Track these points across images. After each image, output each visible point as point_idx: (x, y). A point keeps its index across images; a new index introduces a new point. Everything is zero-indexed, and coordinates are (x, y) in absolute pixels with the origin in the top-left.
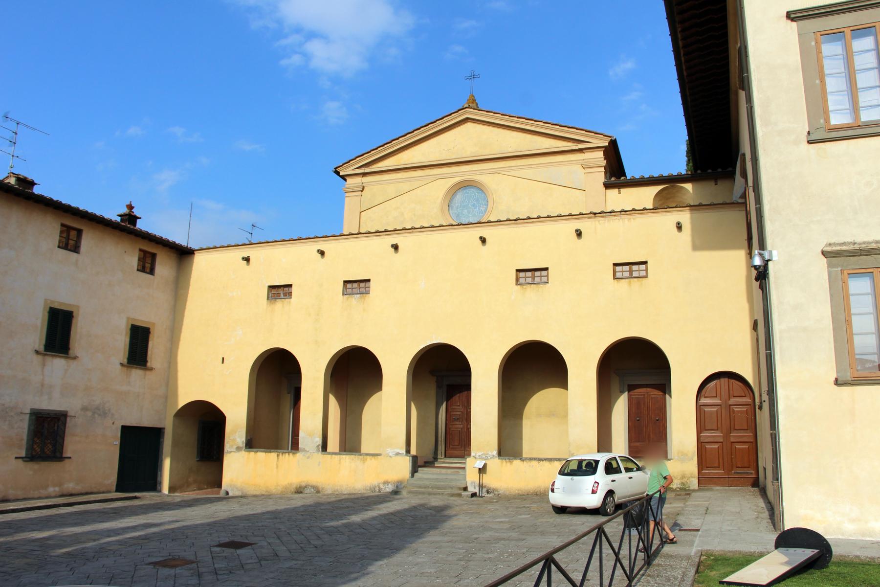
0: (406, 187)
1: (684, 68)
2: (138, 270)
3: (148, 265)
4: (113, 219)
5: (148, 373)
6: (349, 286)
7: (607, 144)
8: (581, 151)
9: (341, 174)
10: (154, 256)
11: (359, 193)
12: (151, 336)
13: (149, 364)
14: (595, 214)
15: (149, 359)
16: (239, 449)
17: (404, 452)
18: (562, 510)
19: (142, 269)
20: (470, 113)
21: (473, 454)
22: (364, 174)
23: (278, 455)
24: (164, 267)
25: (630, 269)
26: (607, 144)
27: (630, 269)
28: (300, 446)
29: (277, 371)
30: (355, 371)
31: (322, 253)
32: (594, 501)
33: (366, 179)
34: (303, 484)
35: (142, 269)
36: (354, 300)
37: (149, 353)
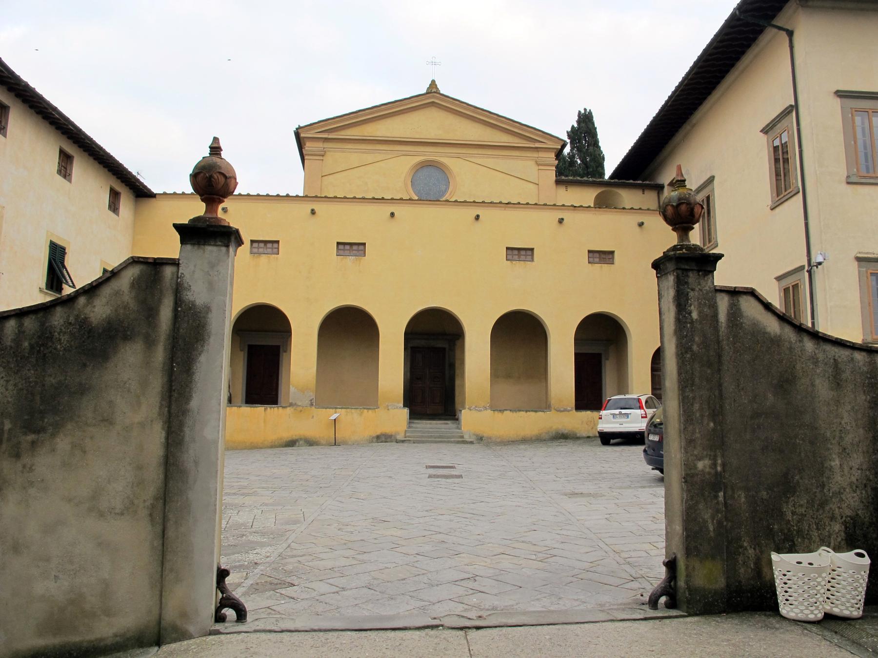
0: (369, 158)
6: (341, 247)
22: (326, 140)
34: (294, 438)
36: (349, 261)
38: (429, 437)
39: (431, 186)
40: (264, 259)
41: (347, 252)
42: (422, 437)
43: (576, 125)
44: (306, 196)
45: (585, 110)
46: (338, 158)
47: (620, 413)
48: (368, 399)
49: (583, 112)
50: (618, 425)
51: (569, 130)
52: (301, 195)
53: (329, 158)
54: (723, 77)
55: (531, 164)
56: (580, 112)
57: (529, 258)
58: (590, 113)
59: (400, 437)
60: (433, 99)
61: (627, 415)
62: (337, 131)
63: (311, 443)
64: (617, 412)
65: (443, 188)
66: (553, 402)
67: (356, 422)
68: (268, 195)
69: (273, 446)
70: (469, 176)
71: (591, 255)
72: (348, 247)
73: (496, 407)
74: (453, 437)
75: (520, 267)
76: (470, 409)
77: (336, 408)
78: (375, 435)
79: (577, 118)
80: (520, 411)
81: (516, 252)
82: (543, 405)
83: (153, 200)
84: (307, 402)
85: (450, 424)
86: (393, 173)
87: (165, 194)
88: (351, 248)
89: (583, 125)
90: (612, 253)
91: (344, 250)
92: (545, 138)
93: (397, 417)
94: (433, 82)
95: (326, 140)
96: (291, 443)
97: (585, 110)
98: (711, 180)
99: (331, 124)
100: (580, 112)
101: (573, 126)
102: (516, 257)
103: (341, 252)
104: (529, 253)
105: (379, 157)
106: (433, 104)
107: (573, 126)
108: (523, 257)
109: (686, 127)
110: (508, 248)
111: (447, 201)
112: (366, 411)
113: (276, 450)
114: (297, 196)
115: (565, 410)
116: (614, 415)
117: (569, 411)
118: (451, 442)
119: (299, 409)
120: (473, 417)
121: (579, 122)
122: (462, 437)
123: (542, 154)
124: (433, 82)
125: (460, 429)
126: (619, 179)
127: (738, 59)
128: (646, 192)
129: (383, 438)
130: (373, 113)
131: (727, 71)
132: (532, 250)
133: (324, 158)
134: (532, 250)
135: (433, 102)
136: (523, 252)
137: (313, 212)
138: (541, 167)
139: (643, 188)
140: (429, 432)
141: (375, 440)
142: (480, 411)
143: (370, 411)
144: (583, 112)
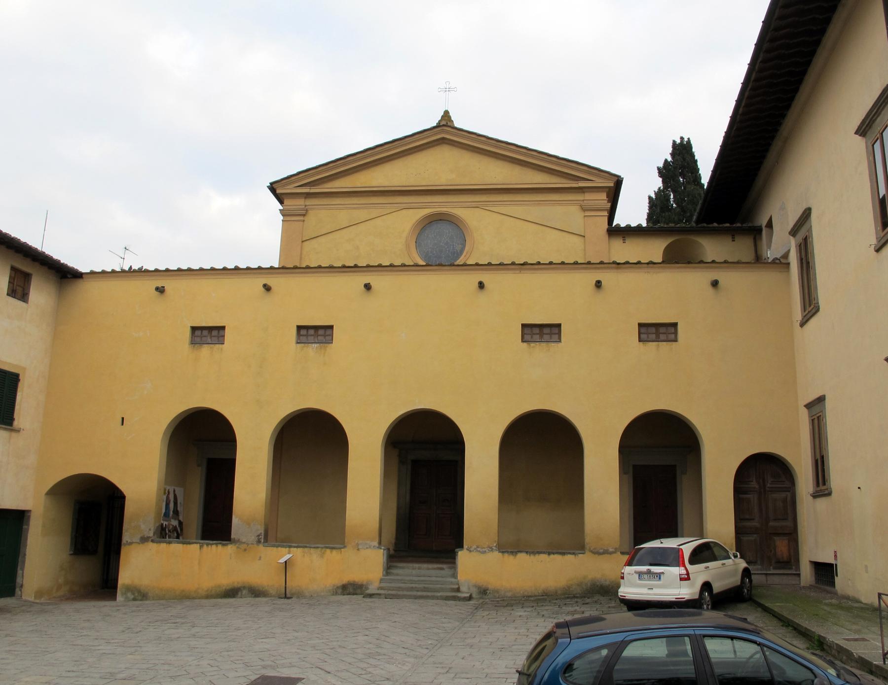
0: (362, 214)
1: (743, 104)
2: (8, 294)
3: (19, 290)
4: (700, 165)
5: (14, 434)
6: (303, 332)
7: (612, 185)
8: (581, 190)
9: (278, 191)
10: (27, 277)
11: (301, 218)
12: (20, 385)
13: (15, 423)
14: (619, 264)
15: (16, 416)
16: (144, 540)
17: (376, 543)
18: (635, 606)
19: (12, 293)
20: (447, 132)
21: (465, 546)
22: (308, 195)
23: (201, 547)
24: (41, 293)
25: (658, 332)
26: (612, 185)
27: (658, 332)
28: (233, 536)
29: (202, 439)
30: (311, 438)
31: (267, 288)
32: (687, 592)
33: (310, 202)
34: (236, 585)
35: (12, 293)
36: (312, 350)
37: (17, 407)
38: (412, 589)
39: (441, 247)
40: (205, 350)
41: (311, 339)
42: (399, 589)
43: (670, 159)
44: (283, 268)
45: (682, 138)
46: (323, 215)
47: (649, 572)
48: (330, 533)
49: (678, 141)
50: (645, 591)
51: (661, 165)
52: (277, 266)
53: (312, 219)
54: (808, 63)
55: (574, 210)
56: (674, 142)
57: (555, 337)
58: (689, 141)
59: (372, 589)
60: (444, 134)
61: (659, 576)
62: (323, 183)
63: (256, 592)
64: (644, 568)
65: (458, 248)
66: (587, 540)
67: (316, 567)
68: (260, 268)
69: (208, 597)
70: (492, 231)
71: (643, 330)
72: (312, 332)
73: (510, 545)
74: (442, 590)
75: (540, 352)
76: (469, 550)
77: (290, 547)
78: (340, 584)
79: (670, 150)
80: (539, 553)
81: (537, 330)
82: (574, 543)
83: (80, 281)
84: (253, 538)
85: (446, 570)
86: (392, 231)
87: (92, 273)
88: (315, 334)
89: (677, 157)
90: (675, 325)
91: (307, 335)
92: (589, 173)
93: (367, 562)
94: (446, 113)
95: (308, 195)
96: (232, 593)
97: (682, 138)
98: (807, 214)
99: (313, 175)
100: (674, 142)
101: (666, 160)
102: (537, 337)
103: (303, 339)
104: (556, 330)
105: (375, 213)
106: (443, 141)
107: (666, 160)
108: (546, 337)
109: (776, 145)
110: (524, 326)
111: (465, 265)
112: (328, 551)
113: (213, 601)
114: (272, 268)
115: (606, 552)
116: (640, 574)
117: (611, 553)
118: (437, 598)
119: (243, 546)
120: (475, 565)
121: (673, 154)
122: (458, 590)
123: (588, 196)
124: (446, 113)
125: (454, 576)
126: (708, 223)
127: (823, 32)
128: (736, 238)
129: (351, 589)
130: (365, 158)
131: (812, 54)
132: (559, 326)
133: (306, 218)
134: (559, 326)
135: (443, 139)
136: (546, 330)
137: (481, 285)
138: (588, 213)
139: (733, 233)
140: (412, 582)
141: (340, 591)
142: (484, 552)
143: (334, 552)
144: (678, 141)
